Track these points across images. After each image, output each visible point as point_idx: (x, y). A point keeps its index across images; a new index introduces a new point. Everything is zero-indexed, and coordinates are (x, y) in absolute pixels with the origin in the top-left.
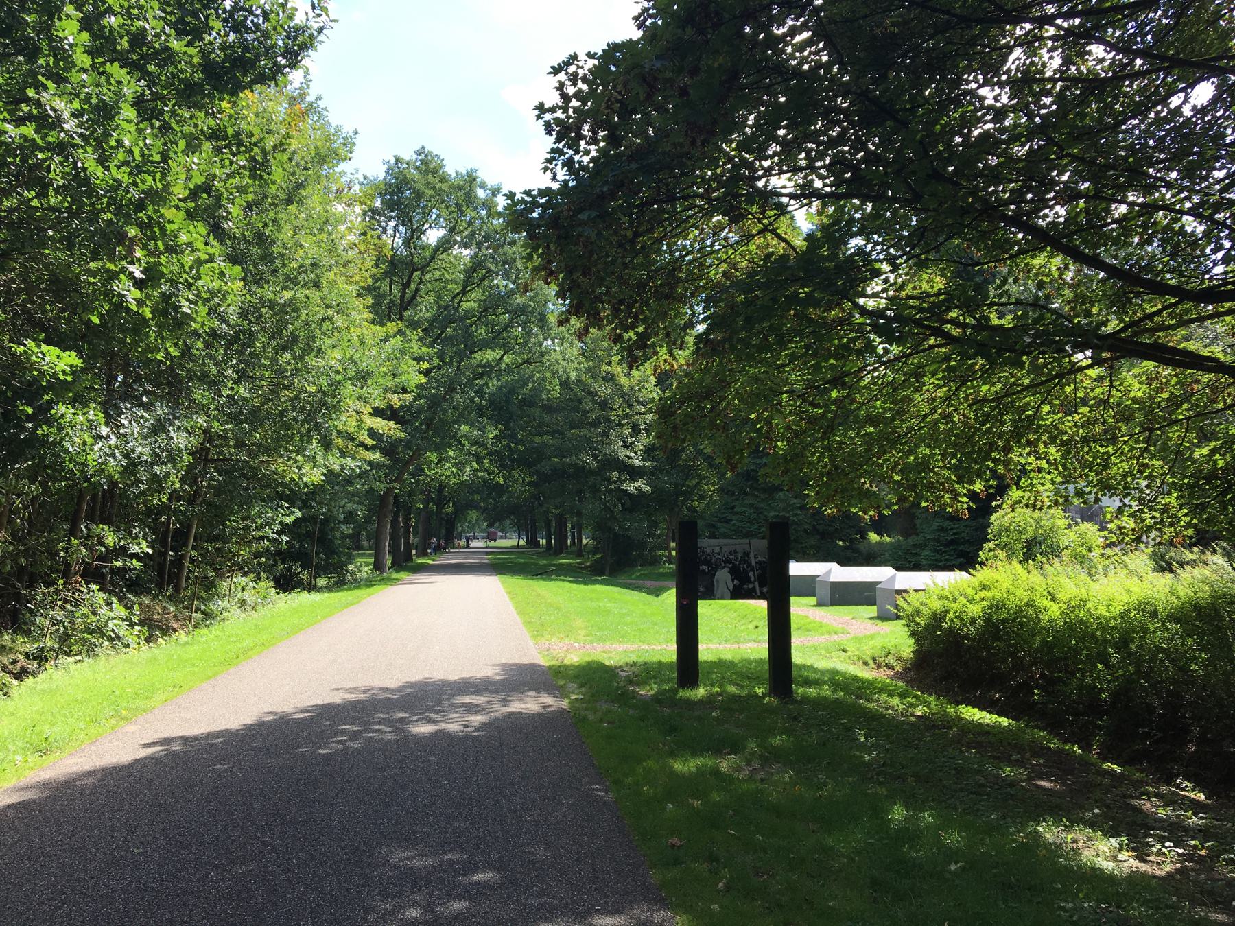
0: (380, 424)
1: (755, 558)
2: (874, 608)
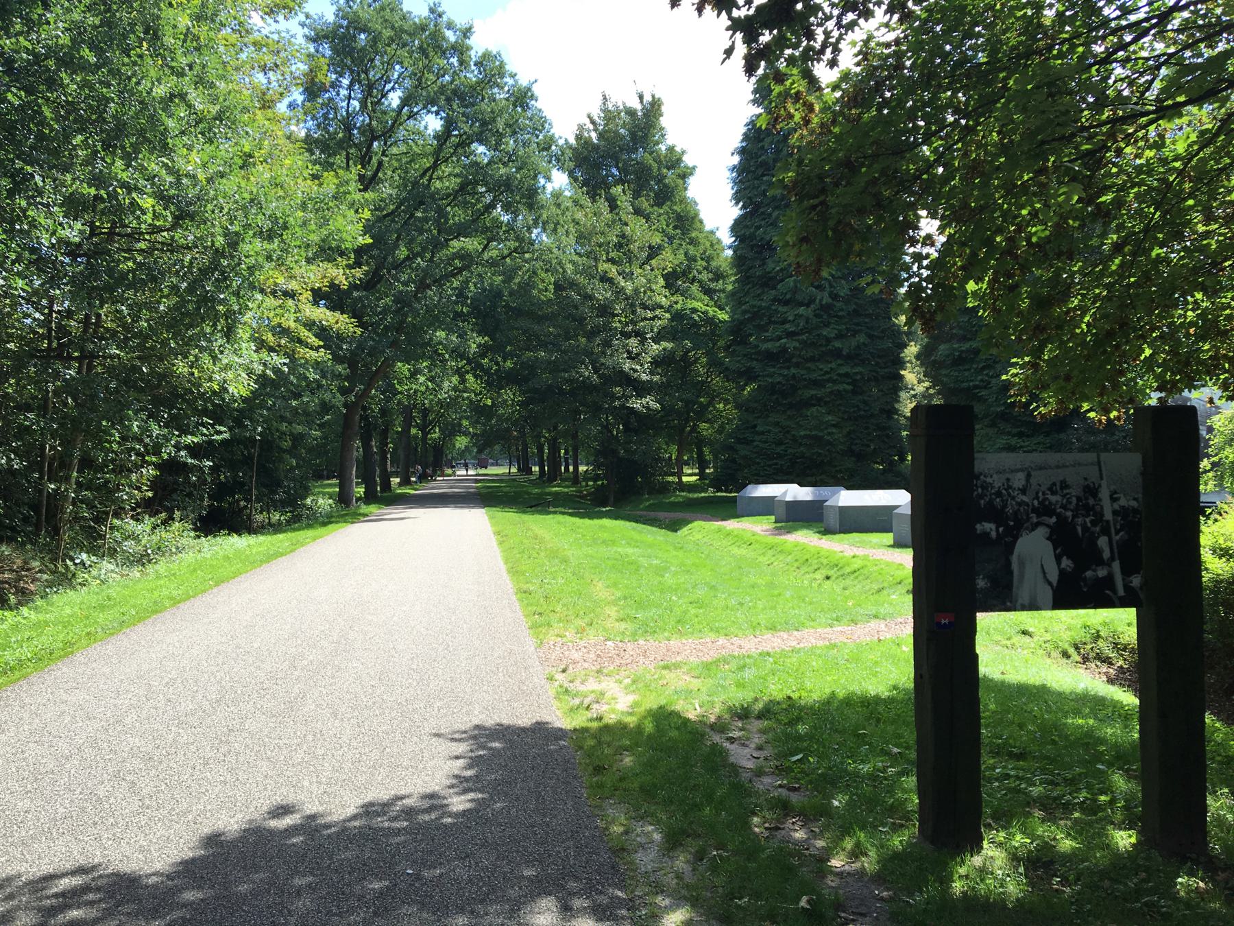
0: (322, 314)
1: (1113, 499)
2: (891, 535)
